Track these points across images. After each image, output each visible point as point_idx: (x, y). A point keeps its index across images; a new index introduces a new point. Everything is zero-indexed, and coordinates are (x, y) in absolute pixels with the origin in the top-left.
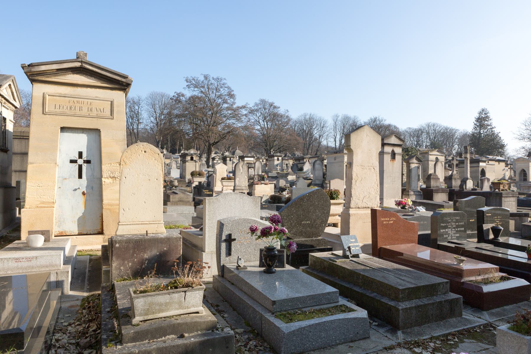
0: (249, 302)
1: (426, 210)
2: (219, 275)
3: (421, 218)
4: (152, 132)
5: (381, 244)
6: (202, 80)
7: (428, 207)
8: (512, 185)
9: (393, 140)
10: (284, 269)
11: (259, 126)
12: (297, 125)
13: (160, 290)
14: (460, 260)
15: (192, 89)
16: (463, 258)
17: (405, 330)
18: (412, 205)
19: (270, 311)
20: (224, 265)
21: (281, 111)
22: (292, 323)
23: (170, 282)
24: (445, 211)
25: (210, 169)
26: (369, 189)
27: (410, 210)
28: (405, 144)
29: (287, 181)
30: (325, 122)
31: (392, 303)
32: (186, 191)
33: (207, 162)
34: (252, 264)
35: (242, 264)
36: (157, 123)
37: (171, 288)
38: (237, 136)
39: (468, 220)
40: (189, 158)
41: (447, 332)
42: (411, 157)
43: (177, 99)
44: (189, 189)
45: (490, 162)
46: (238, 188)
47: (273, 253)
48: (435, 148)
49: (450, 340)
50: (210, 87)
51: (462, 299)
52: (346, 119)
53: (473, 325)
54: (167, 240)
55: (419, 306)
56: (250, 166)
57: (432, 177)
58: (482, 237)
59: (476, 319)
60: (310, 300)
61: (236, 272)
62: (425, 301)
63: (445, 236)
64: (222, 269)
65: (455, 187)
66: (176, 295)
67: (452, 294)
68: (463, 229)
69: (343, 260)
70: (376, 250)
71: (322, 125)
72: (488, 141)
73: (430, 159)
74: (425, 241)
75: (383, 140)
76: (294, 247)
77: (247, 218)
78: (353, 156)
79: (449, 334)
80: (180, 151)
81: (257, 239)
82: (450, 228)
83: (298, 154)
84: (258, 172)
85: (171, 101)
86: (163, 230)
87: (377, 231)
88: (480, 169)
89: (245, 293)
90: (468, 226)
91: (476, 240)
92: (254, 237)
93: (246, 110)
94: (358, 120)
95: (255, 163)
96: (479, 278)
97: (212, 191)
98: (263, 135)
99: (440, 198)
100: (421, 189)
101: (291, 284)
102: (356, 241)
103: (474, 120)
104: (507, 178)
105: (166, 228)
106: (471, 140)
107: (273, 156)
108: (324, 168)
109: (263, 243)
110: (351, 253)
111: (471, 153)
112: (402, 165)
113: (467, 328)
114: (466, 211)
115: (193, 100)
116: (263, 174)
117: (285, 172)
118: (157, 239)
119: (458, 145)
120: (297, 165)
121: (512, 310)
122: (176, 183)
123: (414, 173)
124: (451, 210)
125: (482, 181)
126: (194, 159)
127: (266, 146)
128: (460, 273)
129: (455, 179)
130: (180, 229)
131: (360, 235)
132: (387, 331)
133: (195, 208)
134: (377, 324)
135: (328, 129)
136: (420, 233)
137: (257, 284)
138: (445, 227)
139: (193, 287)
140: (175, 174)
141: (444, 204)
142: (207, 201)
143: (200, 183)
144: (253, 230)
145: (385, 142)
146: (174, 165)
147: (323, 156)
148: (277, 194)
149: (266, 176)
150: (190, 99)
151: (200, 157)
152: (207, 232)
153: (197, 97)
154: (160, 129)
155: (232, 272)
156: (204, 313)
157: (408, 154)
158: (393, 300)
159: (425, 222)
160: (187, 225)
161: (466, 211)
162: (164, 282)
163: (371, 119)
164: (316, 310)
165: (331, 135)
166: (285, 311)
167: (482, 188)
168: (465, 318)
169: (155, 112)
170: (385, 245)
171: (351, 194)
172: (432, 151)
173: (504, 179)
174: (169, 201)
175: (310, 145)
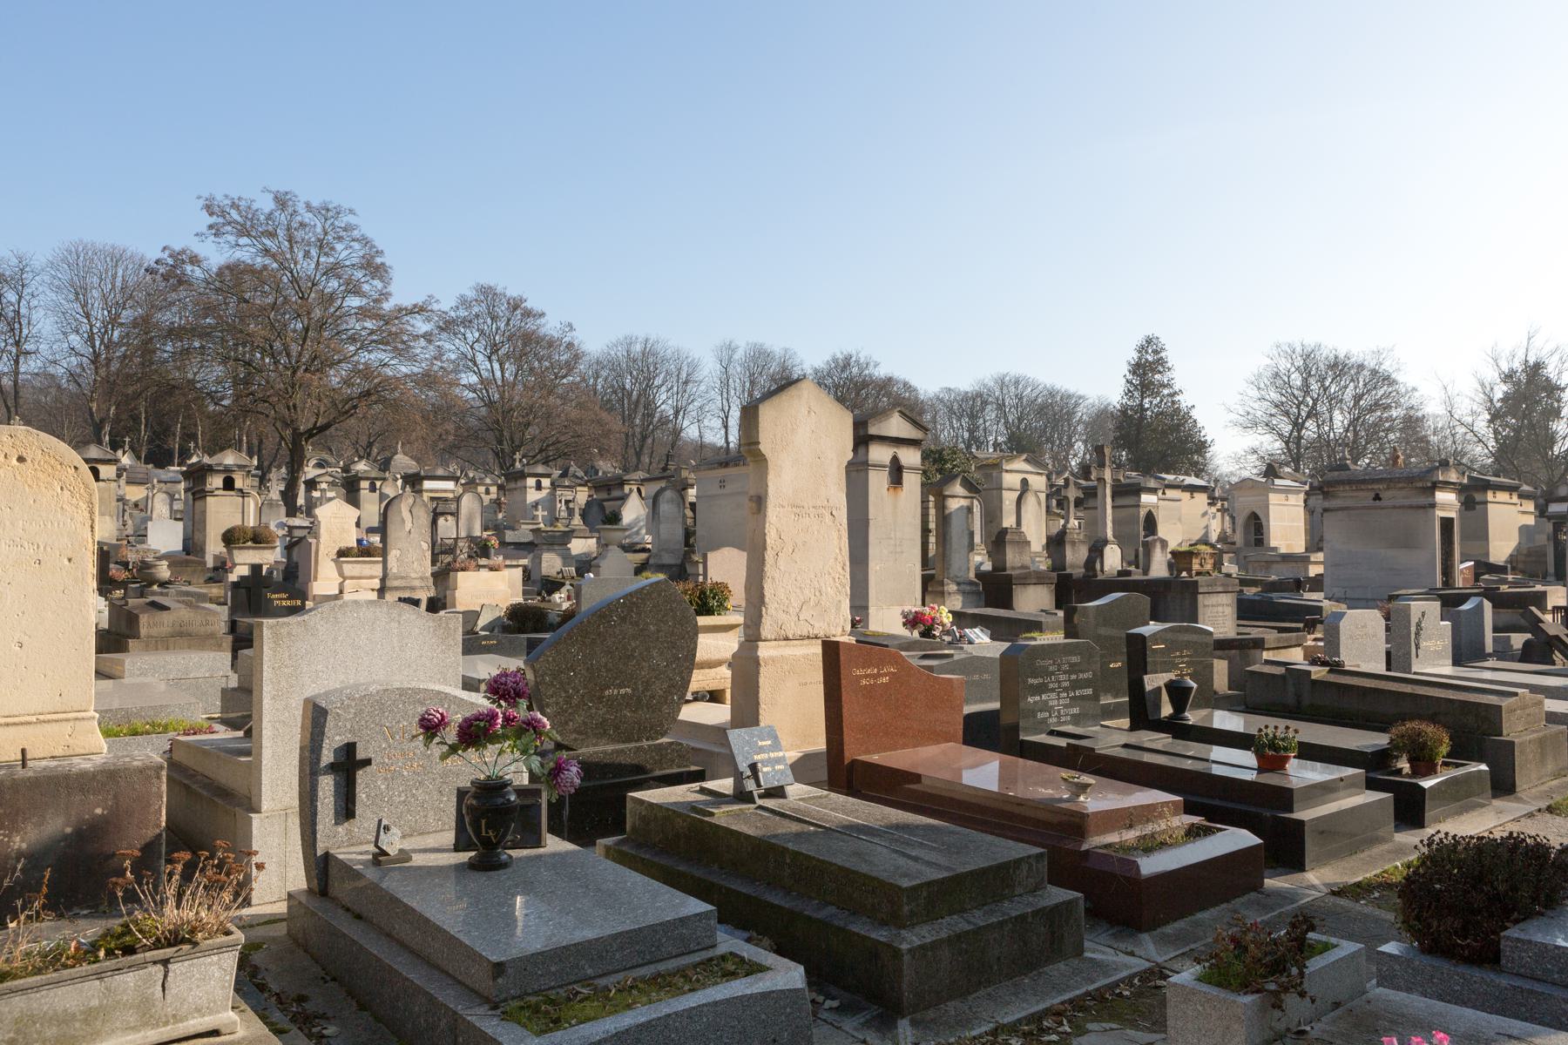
0: (416, 975)
1: (992, 638)
2: (310, 891)
3: (974, 664)
4: (72, 387)
5: (852, 752)
6: (267, 211)
7: (999, 629)
8: (1226, 557)
9: (896, 426)
10: (541, 850)
11: (474, 375)
12: (604, 373)
13: (65, 966)
14: (1077, 784)
15: (231, 238)
16: (1086, 779)
17: (918, 1016)
18: (953, 624)
19: (486, 1000)
20: (327, 855)
21: (550, 326)
22: (559, 1033)
23: (108, 933)
24: (1043, 639)
25: (296, 521)
26: (814, 577)
27: (947, 638)
28: (937, 438)
29: (567, 558)
30: (694, 367)
31: (881, 935)
32: (203, 597)
33: (289, 496)
34: (431, 841)
35: (393, 843)
36: (96, 355)
37: (110, 953)
38: (395, 406)
39: (1104, 666)
40: (216, 481)
41: (1041, 1006)
42: (949, 478)
43: (172, 273)
44: (215, 591)
45: (1170, 493)
46: (396, 583)
47: (500, 801)
48: (1021, 450)
49: (1047, 1031)
50: (299, 235)
51: (1082, 902)
52: (759, 356)
53: (1114, 979)
54: (108, 778)
55: (959, 937)
56: (440, 509)
57: (1008, 537)
58: (1141, 714)
59: (1123, 958)
60: (622, 948)
61: (371, 874)
62: (979, 918)
63: (1040, 716)
64: (322, 868)
65: (1072, 566)
66: (129, 980)
67: (1054, 890)
68: (1089, 691)
69: (736, 807)
70: (840, 771)
71: (684, 376)
72: (1164, 432)
73: (1005, 485)
74: (984, 732)
75: (860, 426)
76: (573, 774)
77: (413, 685)
78: (766, 474)
79: (1047, 1012)
80: (185, 454)
81: (444, 757)
82: (1053, 690)
83: (607, 467)
84: (470, 529)
85: (148, 277)
86: (99, 743)
87: (840, 708)
88: (1143, 513)
89: (403, 945)
90: (1102, 683)
91: (1125, 722)
92: (436, 750)
93: (429, 320)
94: (797, 361)
95: (458, 499)
96: (1130, 836)
97: (303, 595)
98: (490, 404)
99: (1032, 601)
100: (980, 575)
101: (563, 900)
102: (776, 746)
103: (1125, 369)
104: (1214, 537)
105: (107, 734)
106: (1119, 428)
107: (522, 476)
108: (689, 513)
109: (468, 769)
110: (759, 785)
111: (1119, 466)
112: (924, 502)
113: (1097, 990)
114: (1098, 639)
115: (234, 273)
116: (485, 534)
117: (561, 527)
118: (67, 777)
119: (1085, 442)
120: (600, 504)
121: (1214, 921)
122: (164, 571)
123: (956, 527)
124: (1057, 638)
125: (1148, 548)
126: (238, 484)
127: (500, 442)
128: (1077, 825)
129: (1073, 543)
130: (171, 734)
131: (791, 723)
132: (867, 1025)
133: (235, 657)
134: (835, 1004)
135: (703, 388)
136: (968, 709)
137: (447, 911)
138: (1041, 689)
139: (196, 944)
140: (165, 537)
141: (1043, 618)
142: (266, 632)
143: (256, 568)
144: (430, 727)
145: (873, 431)
146: (160, 506)
147: (685, 474)
148: (534, 602)
149: (494, 542)
150: (220, 273)
151: (263, 480)
152: (266, 742)
153: (251, 270)
154: (106, 380)
155: (358, 875)
156: (241, 1033)
157: (941, 469)
158: (883, 923)
159: (986, 676)
160: (200, 718)
161: (1098, 639)
162: (90, 930)
163: (835, 360)
164: (643, 980)
165: (711, 406)
166: (536, 993)
167: (1146, 571)
168: (1091, 959)
169: (88, 316)
170: (868, 752)
171: (762, 596)
172: (1011, 459)
173: (1204, 541)
174: (136, 636)
175: (644, 438)
